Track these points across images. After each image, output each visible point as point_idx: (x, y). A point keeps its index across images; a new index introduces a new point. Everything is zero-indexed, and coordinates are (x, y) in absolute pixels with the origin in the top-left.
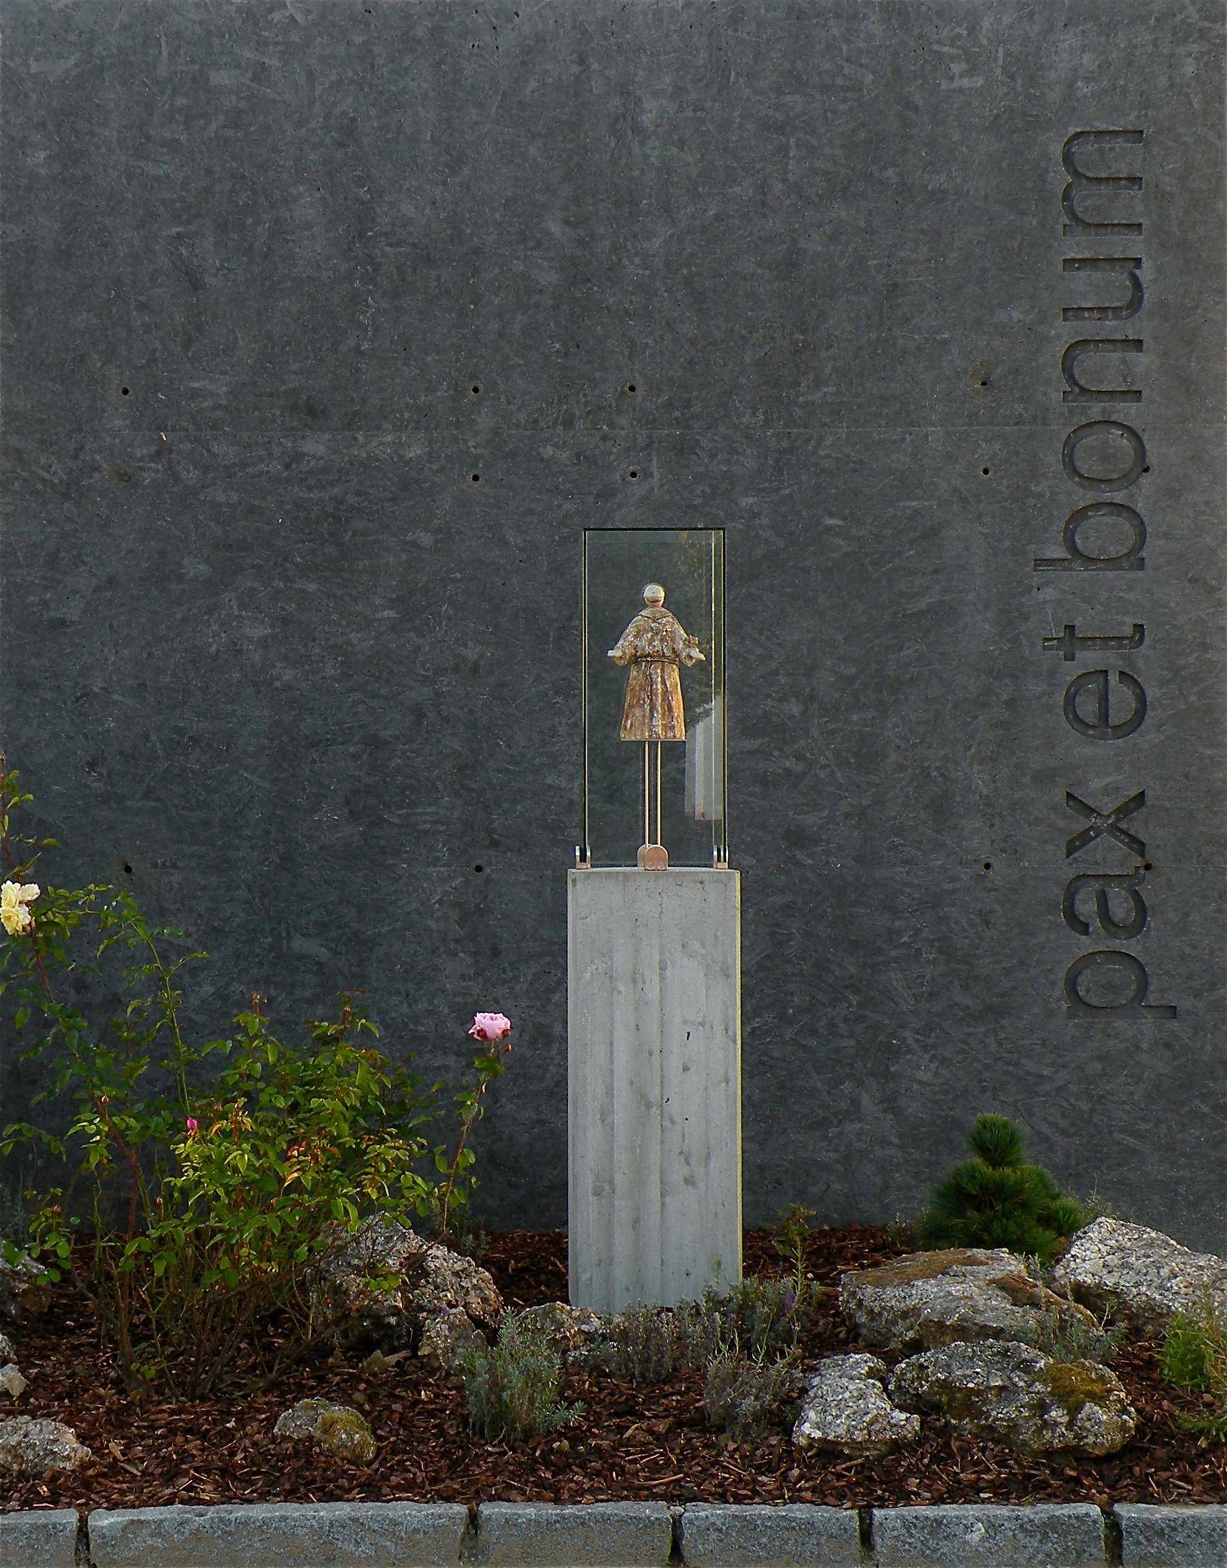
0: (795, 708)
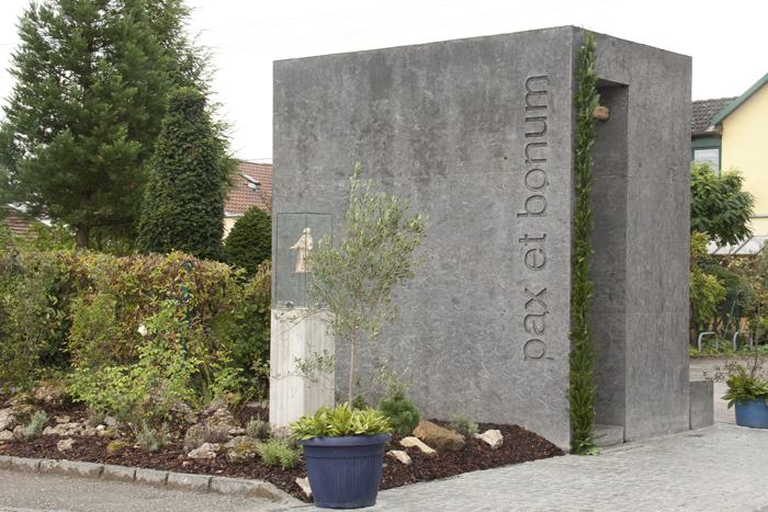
0: (454, 261)
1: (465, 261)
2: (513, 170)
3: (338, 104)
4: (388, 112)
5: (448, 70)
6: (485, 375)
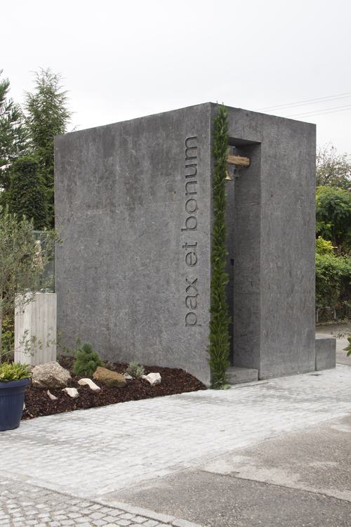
0: (148, 261)
1: (153, 261)
2: (179, 200)
3: (87, 161)
4: (113, 165)
5: (144, 136)
6: (165, 336)
